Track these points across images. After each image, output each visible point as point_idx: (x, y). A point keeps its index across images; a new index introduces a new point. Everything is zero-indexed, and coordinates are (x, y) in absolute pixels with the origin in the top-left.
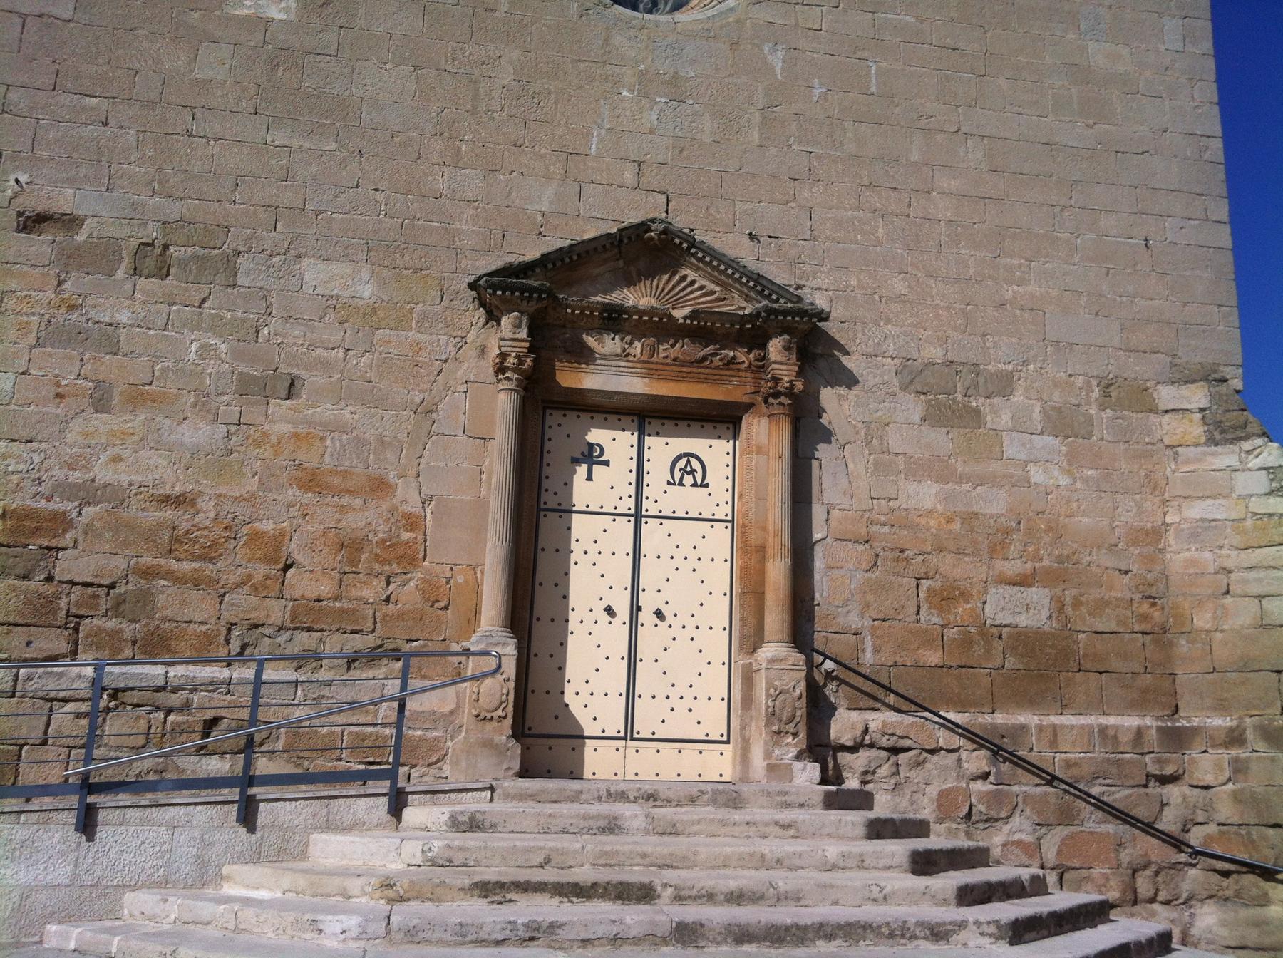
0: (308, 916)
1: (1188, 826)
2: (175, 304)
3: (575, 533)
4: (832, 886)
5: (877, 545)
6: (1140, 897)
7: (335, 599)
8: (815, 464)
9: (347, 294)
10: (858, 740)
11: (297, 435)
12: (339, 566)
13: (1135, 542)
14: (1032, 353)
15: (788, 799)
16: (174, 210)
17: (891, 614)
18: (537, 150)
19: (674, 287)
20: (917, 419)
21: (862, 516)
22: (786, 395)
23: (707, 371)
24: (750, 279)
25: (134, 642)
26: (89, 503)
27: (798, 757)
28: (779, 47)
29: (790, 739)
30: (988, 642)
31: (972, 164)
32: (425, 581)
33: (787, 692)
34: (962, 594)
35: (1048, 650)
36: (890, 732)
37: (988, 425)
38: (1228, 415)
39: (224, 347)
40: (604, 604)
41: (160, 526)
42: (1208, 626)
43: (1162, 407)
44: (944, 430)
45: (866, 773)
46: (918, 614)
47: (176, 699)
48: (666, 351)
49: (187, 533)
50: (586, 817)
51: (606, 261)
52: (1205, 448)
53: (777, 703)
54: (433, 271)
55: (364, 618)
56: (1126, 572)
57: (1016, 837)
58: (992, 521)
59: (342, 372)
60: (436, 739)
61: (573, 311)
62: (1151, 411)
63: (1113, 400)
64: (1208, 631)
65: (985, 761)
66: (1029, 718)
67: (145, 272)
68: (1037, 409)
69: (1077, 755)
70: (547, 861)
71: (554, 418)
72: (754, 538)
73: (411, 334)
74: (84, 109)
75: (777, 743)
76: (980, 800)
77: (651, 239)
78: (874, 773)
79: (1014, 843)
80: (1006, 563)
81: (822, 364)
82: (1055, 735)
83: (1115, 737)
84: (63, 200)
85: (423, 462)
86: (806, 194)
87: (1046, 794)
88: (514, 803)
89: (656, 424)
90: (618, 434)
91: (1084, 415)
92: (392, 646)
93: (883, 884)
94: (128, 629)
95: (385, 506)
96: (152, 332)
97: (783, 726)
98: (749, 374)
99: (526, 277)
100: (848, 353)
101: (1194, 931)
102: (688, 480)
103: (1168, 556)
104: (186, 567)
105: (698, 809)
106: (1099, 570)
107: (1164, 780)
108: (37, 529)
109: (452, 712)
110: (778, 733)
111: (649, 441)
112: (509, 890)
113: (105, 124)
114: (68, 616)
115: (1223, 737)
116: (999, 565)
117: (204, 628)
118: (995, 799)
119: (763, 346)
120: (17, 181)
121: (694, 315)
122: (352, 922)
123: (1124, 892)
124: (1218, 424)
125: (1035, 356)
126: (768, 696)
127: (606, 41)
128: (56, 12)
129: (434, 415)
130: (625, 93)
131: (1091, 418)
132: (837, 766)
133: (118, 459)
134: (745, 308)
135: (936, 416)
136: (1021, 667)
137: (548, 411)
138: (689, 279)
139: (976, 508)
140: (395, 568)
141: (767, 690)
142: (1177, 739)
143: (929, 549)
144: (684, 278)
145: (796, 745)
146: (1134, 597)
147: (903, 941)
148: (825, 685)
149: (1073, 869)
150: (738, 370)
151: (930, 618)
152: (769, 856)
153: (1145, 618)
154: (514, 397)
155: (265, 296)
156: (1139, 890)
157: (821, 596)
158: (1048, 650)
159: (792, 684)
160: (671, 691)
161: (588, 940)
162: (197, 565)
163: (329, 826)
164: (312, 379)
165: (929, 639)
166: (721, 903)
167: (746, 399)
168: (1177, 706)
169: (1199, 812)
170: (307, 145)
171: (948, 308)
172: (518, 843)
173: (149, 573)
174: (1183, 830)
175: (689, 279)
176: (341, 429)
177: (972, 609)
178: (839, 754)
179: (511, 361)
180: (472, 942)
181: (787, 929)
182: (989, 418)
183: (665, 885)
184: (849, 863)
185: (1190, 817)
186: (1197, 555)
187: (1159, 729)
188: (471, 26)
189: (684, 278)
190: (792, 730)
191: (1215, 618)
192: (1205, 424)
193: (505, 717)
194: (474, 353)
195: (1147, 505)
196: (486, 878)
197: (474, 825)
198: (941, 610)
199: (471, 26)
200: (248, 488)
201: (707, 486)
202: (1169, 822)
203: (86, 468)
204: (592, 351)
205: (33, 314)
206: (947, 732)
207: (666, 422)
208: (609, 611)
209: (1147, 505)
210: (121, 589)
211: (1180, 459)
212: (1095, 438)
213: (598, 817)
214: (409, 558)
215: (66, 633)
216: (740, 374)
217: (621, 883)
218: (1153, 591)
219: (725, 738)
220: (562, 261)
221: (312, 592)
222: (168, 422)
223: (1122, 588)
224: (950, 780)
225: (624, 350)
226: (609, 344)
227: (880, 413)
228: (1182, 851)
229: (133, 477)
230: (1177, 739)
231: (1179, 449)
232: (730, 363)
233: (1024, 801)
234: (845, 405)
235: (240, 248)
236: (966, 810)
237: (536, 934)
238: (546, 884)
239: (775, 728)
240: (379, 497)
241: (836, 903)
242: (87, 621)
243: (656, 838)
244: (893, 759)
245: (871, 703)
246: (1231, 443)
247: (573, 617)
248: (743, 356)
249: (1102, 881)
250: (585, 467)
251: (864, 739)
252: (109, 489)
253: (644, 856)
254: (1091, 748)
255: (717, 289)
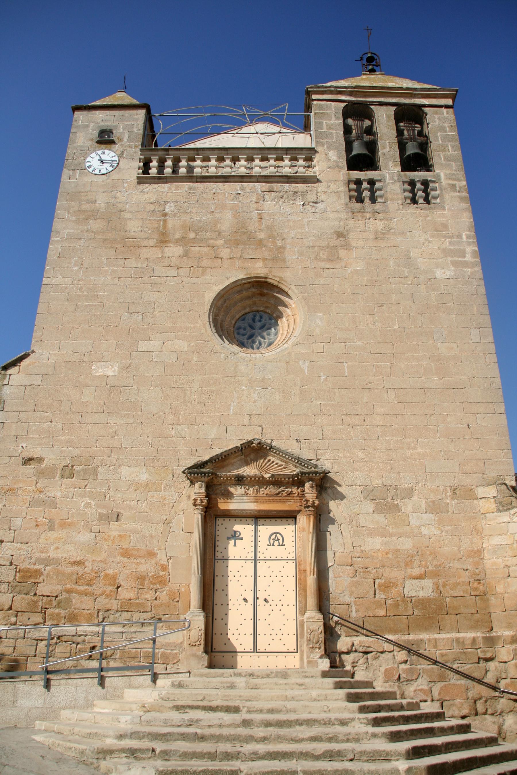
0: (116, 717)
1: (499, 680)
2: (76, 488)
3: (230, 568)
4: (308, 706)
5: (356, 566)
6: (479, 712)
7: (137, 599)
8: (328, 533)
9: (137, 479)
10: (350, 649)
11: (120, 535)
12: (137, 586)
13: (470, 556)
14: (420, 478)
15: (307, 674)
16: (75, 452)
17: (363, 595)
18: (209, 414)
19: (266, 464)
20: (371, 511)
21: (349, 555)
22: (312, 507)
23: (280, 498)
24: (295, 459)
25: (65, 618)
26: (48, 565)
27: (321, 657)
28: (306, 362)
29: (317, 650)
30: (406, 604)
31: (390, 401)
32: (169, 591)
33: (315, 631)
34: (394, 584)
35: (433, 606)
36: (363, 645)
37: (403, 511)
38: (505, 499)
39: (93, 503)
40: (243, 597)
41: (72, 573)
42: (502, 591)
43: (479, 497)
44: (383, 515)
45: (353, 663)
46: (375, 594)
47: (80, 639)
48: (264, 491)
49: (82, 575)
50: (222, 683)
51: (237, 457)
52: (497, 514)
53: (311, 636)
54: (170, 467)
55: (147, 606)
56: (467, 570)
57: (420, 687)
58: (406, 552)
59: (136, 510)
60: (176, 654)
61: (223, 479)
62: (474, 499)
63: (457, 495)
64: (502, 594)
65: (405, 656)
66: (424, 636)
67: (66, 477)
68: (424, 502)
69: (446, 651)
70: (204, 699)
71: (220, 521)
72: (302, 567)
73: (161, 493)
74: (44, 417)
75: (312, 652)
76: (403, 673)
77: (254, 447)
78: (357, 662)
79: (419, 690)
80: (413, 570)
81: (329, 491)
82: (436, 643)
83: (463, 642)
84: (36, 452)
85: (167, 543)
86: (320, 421)
87: (432, 668)
88: (198, 678)
89: (262, 521)
90: (246, 526)
91: (445, 503)
92: (158, 617)
93: (328, 705)
94: (63, 613)
95: (153, 562)
96: (68, 499)
97: (314, 645)
98: (298, 498)
99: (203, 468)
100: (340, 486)
101: (505, 727)
102: (276, 543)
103: (485, 561)
104: (82, 588)
105: (271, 679)
106: (454, 570)
107: (487, 660)
108: (31, 576)
109: (181, 643)
110: (312, 648)
111: (259, 528)
112: (186, 708)
113: (51, 422)
114: (42, 608)
115: (510, 640)
116: (410, 571)
117: (89, 612)
118: (409, 671)
119: (303, 486)
120: (22, 447)
121: (273, 476)
122: (129, 718)
123: (470, 710)
124: (501, 503)
125: (422, 480)
126: (308, 633)
127: (236, 367)
128: (35, 383)
129: (171, 524)
130: (243, 388)
131: (448, 504)
132: (341, 660)
133: (57, 548)
134: (295, 471)
135: (379, 509)
136: (421, 614)
137: (217, 519)
138: (272, 461)
139: (399, 547)
140: (158, 586)
141: (307, 630)
142: (491, 641)
143: (379, 566)
144: (269, 460)
145: (320, 652)
146: (470, 580)
147: (329, 726)
148: (335, 627)
149: (447, 700)
150: (294, 497)
151: (380, 596)
152: (289, 696)
153: (476, 589)
154: (200, 516)
155: (108, 482)
156: (478, 709)
157: (333, 589)
158: (433, 606)
159: (317, 627)
160: (272, 632)
161: (211, 726)
162: (86, 587)
163: (130, 686)
164: (125, 514)
165: (378, 605)
166: (265, 713)
167: (297, 509)
168: (492, 627)
169: (503, 673)
170: (122, 422)
171: (383, 463)
172: (193, 692)
173: (69, 591)
174: (497, 682)
175: (272, 461)
176: (136, 532)
177: (399, 591)
178: (342, 656)
179: (198, 502)
180: (170, 726)
181: (284, 722)
182: (403, 508)
183: (244, 707)
184: (321, 698)
185: (499, 676)
186: (496, 560)
187: (483, 637)
188: (183, 369)
189: (269, 460)
190: (318, 646)
191: (504, 587)
192: (496, 503)
193: (200, 645)
194: (186, 498)
195: (475, 540)
196: (178, 704)
197: (180, 686)
198: (384, 592)
199: (183, 369)
200: (103, 557)
201: (284, 545)
202: (490, 679)
203: (47, 552)
204: (232, 494)
205: (28, 496)
206: (388, 644)
207: (266, 519)
208: (245, 600)
209: (475, 540)
210: (60, 598)
211: (487, 519)
212: (450, 513)
213: (227, 682)
214: (163, 582)
215: (42, 614)
216: (294, 498)
217: (227, 706)
218: (479, 577)
219: (296, 651)
220: (218, 459)
221: (128, 598)
222: (74, 533)
223: (465, 577)
224: (390, 664)
225: (246, 492)
226: (238, 490)
227: (355, 510)
228: (496, 691)
229: (63, 555)
230: (491, 641)
231: (486, 514)
232: (290, 494)
233: (423, 672)
234: (340, 507)
235: (99, 465)
236: (397, 676)
237: (192, 723)
238: (199, 706)
239: (311, 646)
240: (151, 558)
241: (310, 713)
242: (49, 610)
243: (250, 690)
244: (365, 656)
245: (355, 633)
246: (506, 511)
247: (230, 603)
248: (295, 490)
249: (460, 706)
250: (233, 540)
251: (352, 649)
252: (55, 560)
253: (240, 696)
254: (452, 647)
255: (283, 463)
